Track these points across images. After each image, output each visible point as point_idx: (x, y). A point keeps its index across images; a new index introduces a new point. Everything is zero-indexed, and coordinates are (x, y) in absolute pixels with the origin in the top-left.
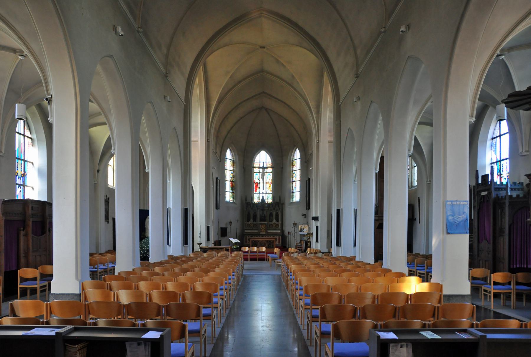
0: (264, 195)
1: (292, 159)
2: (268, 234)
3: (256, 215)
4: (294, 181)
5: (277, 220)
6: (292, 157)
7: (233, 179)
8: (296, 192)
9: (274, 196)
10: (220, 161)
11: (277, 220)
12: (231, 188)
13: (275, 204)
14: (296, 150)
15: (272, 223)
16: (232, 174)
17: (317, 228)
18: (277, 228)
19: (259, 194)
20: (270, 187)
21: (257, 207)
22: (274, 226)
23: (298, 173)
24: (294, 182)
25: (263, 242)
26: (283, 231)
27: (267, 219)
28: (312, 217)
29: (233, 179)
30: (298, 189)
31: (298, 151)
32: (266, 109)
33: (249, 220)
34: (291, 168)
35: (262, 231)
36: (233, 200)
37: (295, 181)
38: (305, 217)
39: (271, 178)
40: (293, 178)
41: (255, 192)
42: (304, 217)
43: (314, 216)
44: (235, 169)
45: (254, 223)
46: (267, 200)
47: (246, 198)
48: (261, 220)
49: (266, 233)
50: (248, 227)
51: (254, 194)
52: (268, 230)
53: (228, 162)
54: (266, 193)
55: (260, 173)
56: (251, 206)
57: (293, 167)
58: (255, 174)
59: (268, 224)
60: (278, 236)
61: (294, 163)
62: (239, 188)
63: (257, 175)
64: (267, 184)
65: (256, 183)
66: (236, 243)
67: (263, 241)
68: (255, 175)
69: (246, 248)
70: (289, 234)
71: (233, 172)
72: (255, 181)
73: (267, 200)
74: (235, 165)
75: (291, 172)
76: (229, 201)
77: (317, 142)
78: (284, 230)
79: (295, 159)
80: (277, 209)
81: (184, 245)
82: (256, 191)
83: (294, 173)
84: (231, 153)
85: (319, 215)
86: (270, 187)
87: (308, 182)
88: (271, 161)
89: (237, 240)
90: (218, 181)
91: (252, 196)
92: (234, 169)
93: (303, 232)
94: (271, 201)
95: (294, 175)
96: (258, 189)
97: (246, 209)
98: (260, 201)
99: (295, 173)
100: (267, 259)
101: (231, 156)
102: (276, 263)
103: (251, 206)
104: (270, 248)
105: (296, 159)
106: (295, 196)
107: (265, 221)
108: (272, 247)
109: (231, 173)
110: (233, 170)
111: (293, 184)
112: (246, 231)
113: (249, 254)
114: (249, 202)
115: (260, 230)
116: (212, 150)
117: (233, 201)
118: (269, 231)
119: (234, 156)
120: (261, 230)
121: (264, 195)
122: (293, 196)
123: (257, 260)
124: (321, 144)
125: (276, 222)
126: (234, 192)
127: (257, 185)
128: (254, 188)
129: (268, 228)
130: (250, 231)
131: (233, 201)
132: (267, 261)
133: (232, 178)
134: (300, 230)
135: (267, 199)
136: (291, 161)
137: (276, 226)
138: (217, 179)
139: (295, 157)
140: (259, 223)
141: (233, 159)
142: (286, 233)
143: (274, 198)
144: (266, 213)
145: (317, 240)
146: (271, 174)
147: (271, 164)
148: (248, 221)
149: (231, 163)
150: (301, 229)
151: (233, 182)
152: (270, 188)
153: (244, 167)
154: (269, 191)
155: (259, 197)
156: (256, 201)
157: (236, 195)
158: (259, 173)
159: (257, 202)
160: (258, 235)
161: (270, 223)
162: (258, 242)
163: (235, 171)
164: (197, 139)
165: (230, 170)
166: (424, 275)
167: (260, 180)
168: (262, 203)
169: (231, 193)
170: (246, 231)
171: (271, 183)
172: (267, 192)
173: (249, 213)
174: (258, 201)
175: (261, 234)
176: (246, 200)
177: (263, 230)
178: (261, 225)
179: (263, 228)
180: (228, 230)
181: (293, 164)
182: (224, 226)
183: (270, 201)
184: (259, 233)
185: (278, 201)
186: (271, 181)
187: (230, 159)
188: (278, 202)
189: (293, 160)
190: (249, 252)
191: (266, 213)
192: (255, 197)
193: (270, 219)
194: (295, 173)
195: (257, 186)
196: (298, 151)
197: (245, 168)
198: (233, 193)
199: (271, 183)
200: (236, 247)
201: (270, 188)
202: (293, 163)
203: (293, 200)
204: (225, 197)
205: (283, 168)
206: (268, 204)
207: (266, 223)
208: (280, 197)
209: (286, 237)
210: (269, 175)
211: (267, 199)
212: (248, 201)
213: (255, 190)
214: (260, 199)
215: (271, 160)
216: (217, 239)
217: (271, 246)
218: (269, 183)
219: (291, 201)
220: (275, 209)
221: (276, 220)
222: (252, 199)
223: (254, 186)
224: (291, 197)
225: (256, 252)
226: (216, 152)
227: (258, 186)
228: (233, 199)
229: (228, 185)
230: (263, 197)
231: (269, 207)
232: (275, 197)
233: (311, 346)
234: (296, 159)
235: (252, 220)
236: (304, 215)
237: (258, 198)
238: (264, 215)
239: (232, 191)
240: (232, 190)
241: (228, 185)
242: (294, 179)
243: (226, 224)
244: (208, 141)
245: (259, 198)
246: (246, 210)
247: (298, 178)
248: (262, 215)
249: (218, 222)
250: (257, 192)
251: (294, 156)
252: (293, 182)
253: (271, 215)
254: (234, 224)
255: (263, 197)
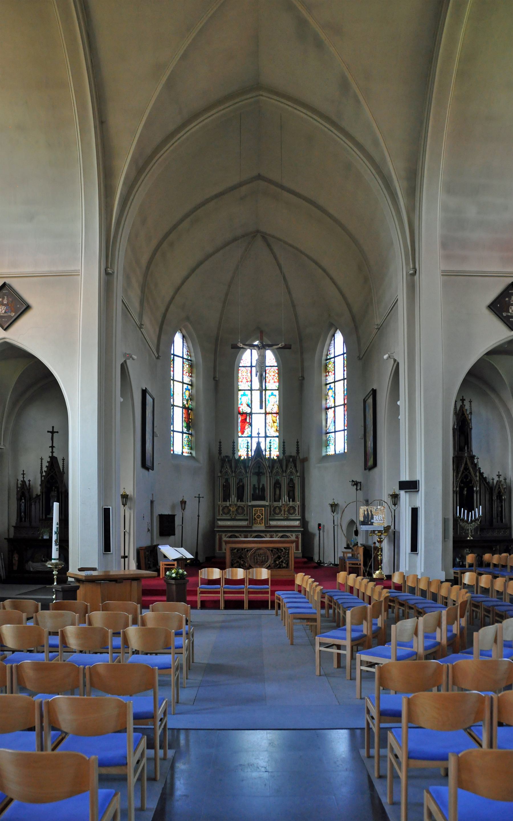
0: (262, 440)
1: (324, 358)
2: (270, 531)
3: (243, 487)
4: (331, 408)
5: (292, 497)
6: (325, 353)
7: (190, 403)
8: (335, 432)
9: (284, 442)
10: (157, 356)
11: (292, 497)
12: (185, 424)
13: (288, 462)
14: (334, 336)
15: (280, 504)
16: (187, 393)
17: (415, 512)
18: (291, 514)
19: (250, 438)
20: (274, 422)
21: (245, 468)
22: (284, 510)
23: (340, 389)
24: (330, 410)
25: (262, 551)
26: (304, 523)
27: (268, 493)
28: (400, 482)
29: (190, 403)
30: (340, 424)
31: (339, 338)
32: (265, 237)
33: (226, 497)
34: (323, 378)
35: (257, 523)
36: (189, 451)
37: (333, 406)
38: (360, 489)
39: (278, 403)
40: (328, 401)
41: (240, 434)
42: (357, 490)
43: (405, 477)
44: (194, 380)
45: (239, 503)
46: (268, 453)
47: (220, 448)
48: (255, 498)
49: (266, 527)
50: (226, 514)
51: (240, 439)
52: (270, 520)
53: (178, 362)
54: (266, 437)
55: (251, 390)
56: (231, 467)
57: (327, 376)
58: (240, 393)
59: (270, 506)
60: (294, 534)
61: (331, 366)
62: (202, 425)
63: (244, 395)
64: (269, 417)
65: (244, 413)
66: (181, 561)
67: (259, 549)
68: (239, 397)
69: (212, 572)
70: (319, 529)
71: (189, 387)
72: (240, 409)
73: (268, 453)
74: (194, 370)
75: (324, 387)
76: (180, 453)
77: (411, 272)
78: (307, 520)
79: (332, 356)
80: (291, 472)
81: (104, 553)
82: (243, 433)
83: (330, 388)
84: (185, 344)
85: (420, 476)
86: (274, 422)
87: (370, 401)
88: (276, 364)
89: (182, 550)
90: (149, 399)
91: (234, 442)
92: (191, 381)
93: (372, 524)
94: (278, 453)
95: (331, 393)
96: (246, 427)
97: (221, 472)
98: (251, 454)
99: (332, 389)
100: (273, 602)
101: (185, 350)
102: (318, 648)
103: (231, 467)
104: (279, 568)
105: (335, 357)
106: (332, 442)
107: (263, 498)
108: (284, 565)
109: (184, 390)
110: (190, 383)
111: (327, 414)
112: (220, 523)
113: (222, 587)
114: (227, 457)
115: (253, 521)
116: (120, 304)
117: (189, 455)
118: (273, 523)
119: (192, 350)
120: (255, 519)
121: (262, 440)
122: (327, 440)
123: (246, 605)
124: (423, 277)
125: (289, 501)
126: (193, 433)
127: (246, 419)
128: (239, 424)
129: (270, 514)
130: (229, 523)
131: (191, 453)
132: (273, 607)
133: (187, 400)
134: (362, 519)
135: (268, 450)
136: (324, 362)
137: (289, 511)
138: (144, 392)
139: (332, 351)
140: (250, 504)
141: (189, 358)
142: (313, 527)
143: (283, 447)
144: (267, 482)
145: (414, 548)
146: (277, 393)
147: (277, 371)
148: (225, 500)
149: (186, 367)
150: (364, 516)
151: (191, 410)
152: (276, 424)
153: (214, 378)
154: (272, 431)
155: (250, 444)
156: (242, 453)
157: (196, 439)
158: (250, 392)
159: (246, 458)
160: (246, 532)
161: (276, 504)
162: (248, 551)
163: (194, 384)
164: (77, 268)
165: (183, 383)
166: (458, 575)
167: (251, 408)
168: (256, 459)
169: (185, 435)
170: (220, 523)
171: (276, 413)
172: (268, 435)
173: (227, 480)
174: (247, 454)
175: (254, 529)
176: (220, 453)
177: (259, 519)
178: (254, 509)
179: (259, 517)
180: (178, 521)
181: (326, 369)
182: (167, 512)
183: (275, 453)
184: (251, 527)
185: (294, 453)
186: (276, 409)
187: (183, 358)
188: (294, 456)
189: (327, 360)
190: (223, 582)
191: (267, 482)
192: (242, 446)
193: (275, 494)
194: (332, 389)
195: (244, 421)
196: (339, 338)
197: (217, 379)
198: (191, 434)
199: (276, 413)
200: (177, 573)
201: (276, 424)
202: (326, 366)
203: (328, 450)
204: (168, 442)
205: (303, 378)
206: (272, 461)
207: (267, 504)
208: (298, 445)
209: (312, 535)
210: (272, 395)
211: (268, 450)
212: (224, 454)
213: (241, 429)
214: (251, 450)
215: (277, 361)
216: (146, 543)
217: (282, 562)
218: (272, 413)
219: (324, 454)
220: (286, 471)
221: (289, 496)
222: (234, 448)
223: (240, 420)
224: (324, 444)
225: (241, 582)
226: (141, 324)
227: (248, 421)
228: (191, 449)
229: (178, 415)
230: (258, 444)
231: (273, 467)
232: (285, 444)
233: (320, 676)
234: (335, 357)
235: (234, 498)
236: (356, 484)
237: (248, 448)
238: (261, 486)
239: (188, 430)
240: (188, 427)
241: (178, 415)
242: (330, 403)
243: (173, 507)
244: (107, 273)
245: (250, 447)
246: (219, 474)
247: (340, 399)
248: (257, 486)
249: (152, 502)
250: (245, 434)
251: (328, 350)
252: (327, 409)
253: (277, 485)
254: (191, 506)
255: (258, 444)
